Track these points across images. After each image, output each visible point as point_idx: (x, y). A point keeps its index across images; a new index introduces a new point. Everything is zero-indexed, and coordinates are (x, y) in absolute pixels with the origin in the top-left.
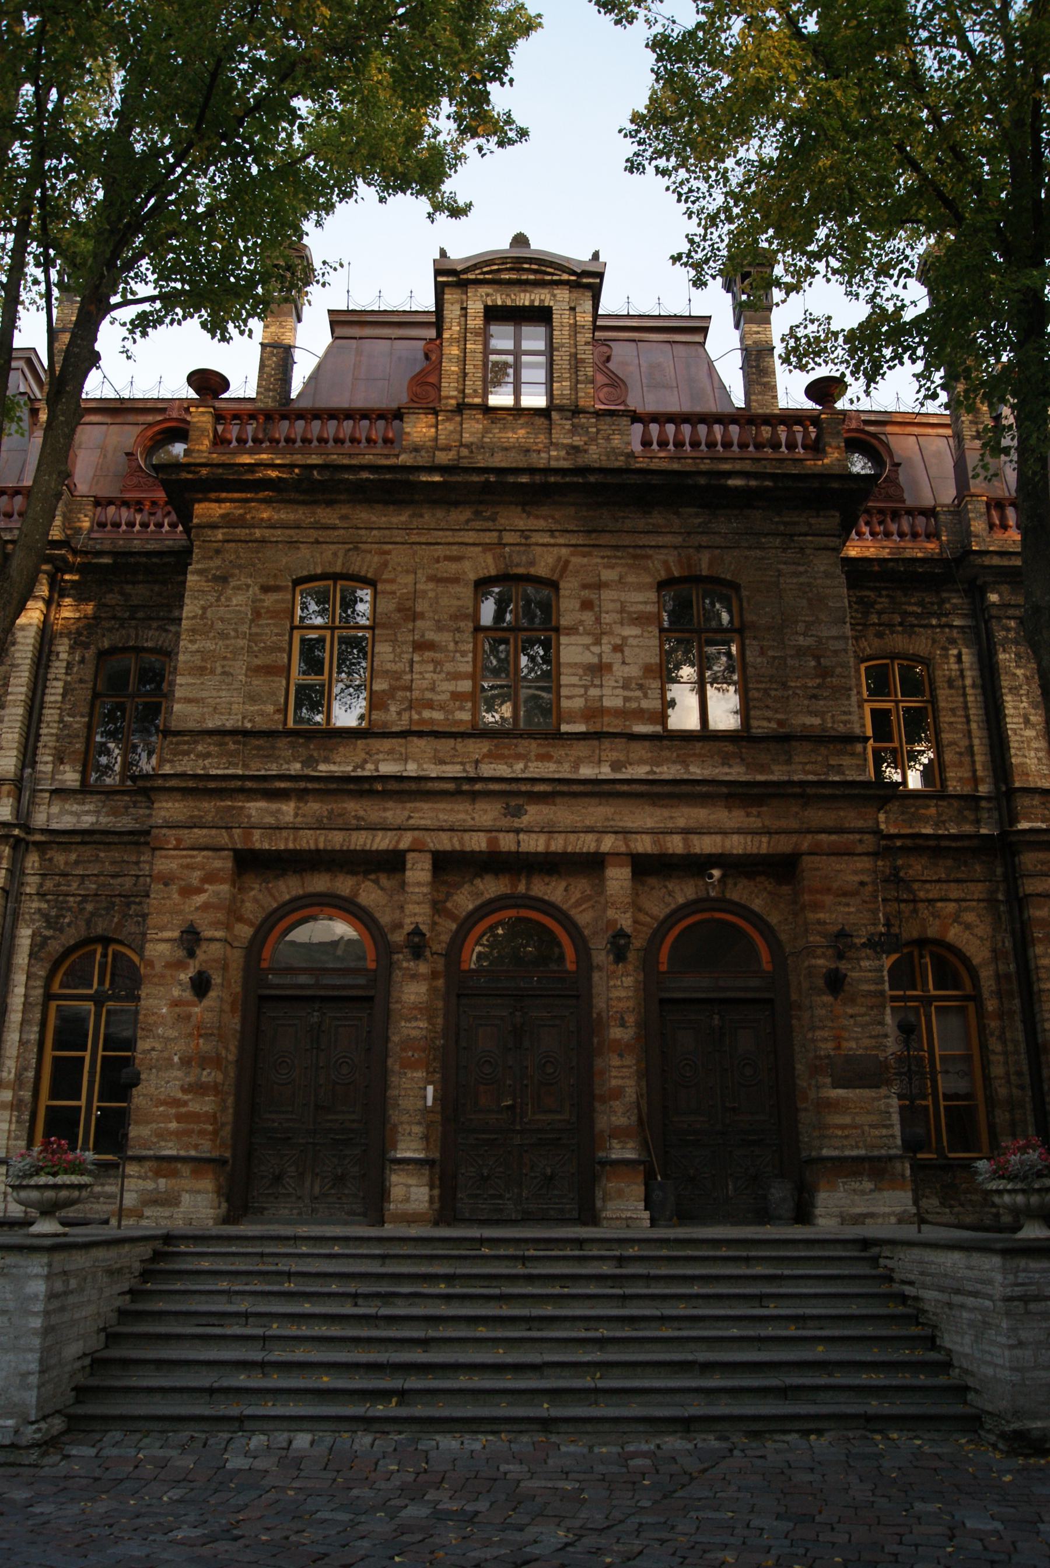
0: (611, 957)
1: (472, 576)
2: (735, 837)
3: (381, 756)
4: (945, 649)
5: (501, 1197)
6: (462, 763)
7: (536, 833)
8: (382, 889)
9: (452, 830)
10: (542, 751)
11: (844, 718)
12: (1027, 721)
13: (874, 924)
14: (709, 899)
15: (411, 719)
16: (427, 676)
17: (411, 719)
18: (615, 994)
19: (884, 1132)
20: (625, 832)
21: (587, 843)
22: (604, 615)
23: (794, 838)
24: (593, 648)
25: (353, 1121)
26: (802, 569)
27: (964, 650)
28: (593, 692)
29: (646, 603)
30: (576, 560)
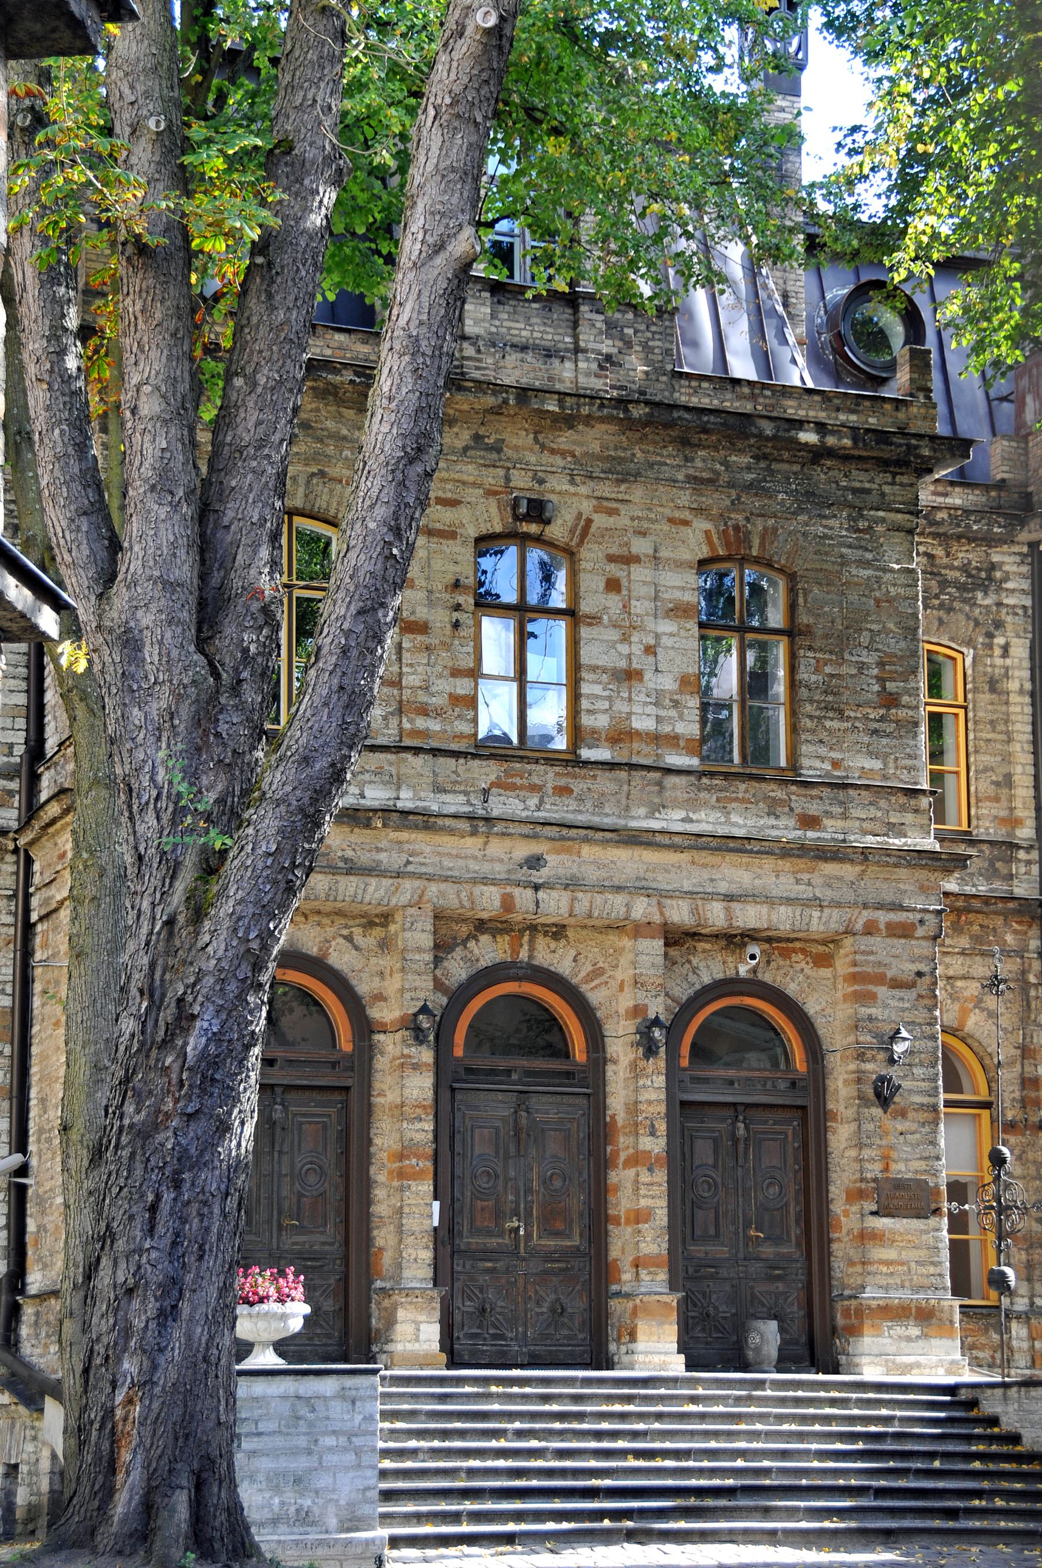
0: (641, 1050)
1: (472, 532)
2: (783, 909)
3: (367, 777)
4: (990, 636)
5: (502, 1337)
6: (466, 793)
8: (357, 948)
10: (562, 782)
11: (909, 762)
13: (930, 1024)
15: (401, 730)
16: (420, 669)
17: (401, 730)
18: (644, 1096)
19: (932, 1270)
22: (633, 602)
23: (847, 914)
24: (620, 647)
25: (324, 1243)
26: (869, 556)
27: (1014, 641)
28: (621, 707)
29: (683, 589)
30: (600, 521)
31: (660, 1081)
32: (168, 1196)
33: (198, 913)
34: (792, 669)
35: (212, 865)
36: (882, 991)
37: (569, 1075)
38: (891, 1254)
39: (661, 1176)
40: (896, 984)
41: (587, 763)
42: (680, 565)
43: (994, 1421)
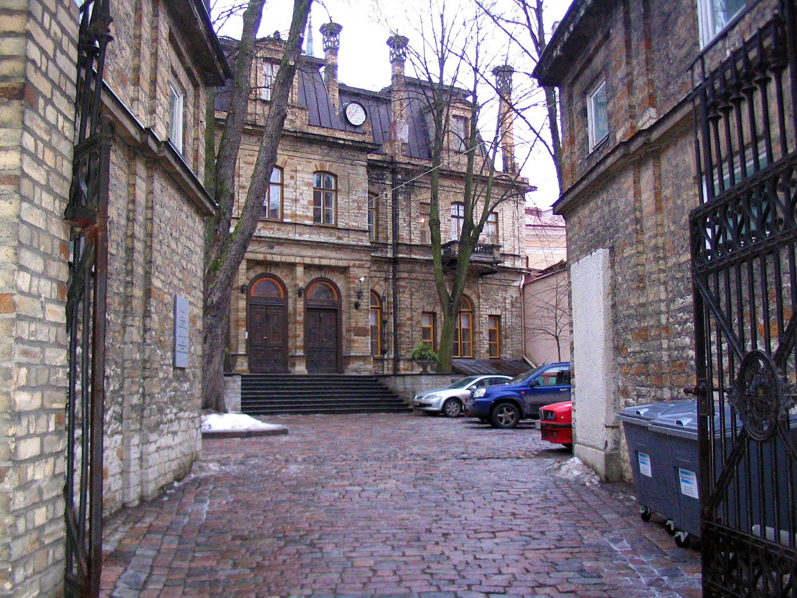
7: (278, 255)
20: (303, 257)
21: (292, 259)
28: (294, 208)
30: (289, 161)
31: (302, 303)
39: (302, 326)
41: (285, 223)
42: (308, 173)
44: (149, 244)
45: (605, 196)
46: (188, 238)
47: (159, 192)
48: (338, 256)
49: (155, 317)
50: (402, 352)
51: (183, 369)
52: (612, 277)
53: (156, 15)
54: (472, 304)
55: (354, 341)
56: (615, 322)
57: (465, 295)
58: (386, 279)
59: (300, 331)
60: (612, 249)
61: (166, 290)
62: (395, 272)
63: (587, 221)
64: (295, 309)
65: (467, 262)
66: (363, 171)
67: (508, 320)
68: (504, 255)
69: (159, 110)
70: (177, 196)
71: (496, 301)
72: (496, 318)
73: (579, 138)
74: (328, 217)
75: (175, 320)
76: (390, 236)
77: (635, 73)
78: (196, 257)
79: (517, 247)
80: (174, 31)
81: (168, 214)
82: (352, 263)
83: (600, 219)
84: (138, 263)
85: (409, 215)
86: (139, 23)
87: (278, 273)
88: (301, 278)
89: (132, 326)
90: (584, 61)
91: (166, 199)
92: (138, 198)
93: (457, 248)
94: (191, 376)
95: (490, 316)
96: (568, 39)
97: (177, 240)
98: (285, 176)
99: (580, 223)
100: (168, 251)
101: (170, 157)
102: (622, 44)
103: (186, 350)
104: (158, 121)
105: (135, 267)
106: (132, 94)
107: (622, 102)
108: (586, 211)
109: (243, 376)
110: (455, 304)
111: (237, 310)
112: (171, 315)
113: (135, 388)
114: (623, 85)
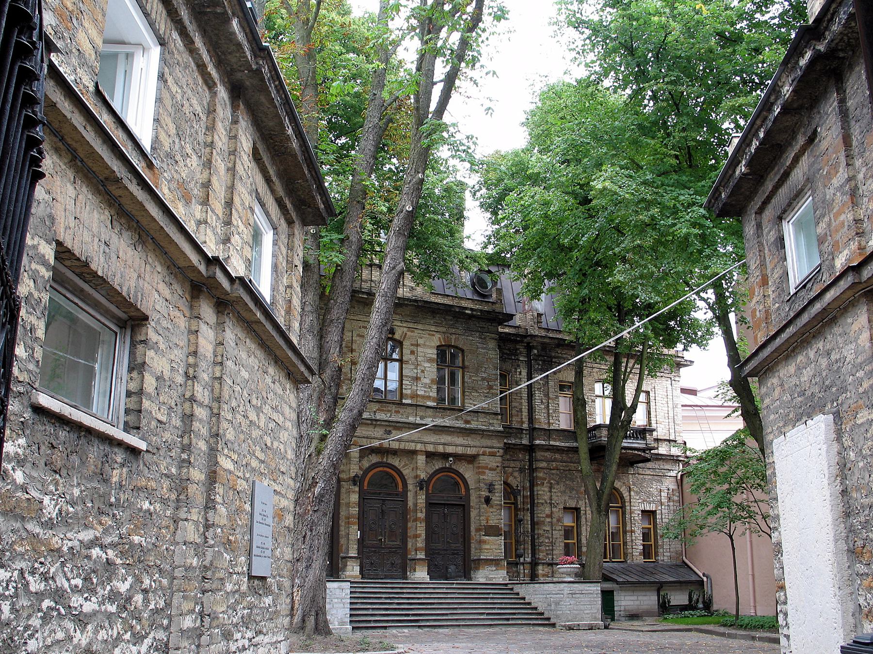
7: (394, 440)
9: (367, 438)
12: (542, 402)
14: (445, 468)
21: (412, 446)
23: (477, 449)
31: (424, 497)
32: (309, 533)
33: (319, 452)
34: (463, 378)
35: (323, 438)
36: (487, 471)
37: (397, 495)
38: (488, 547)
39: (424, 524)
40: (491, 469)
42: (431, 347)
43: (518, 594)
44: (215, 411)
45: (820, 345)
46: (274, 409)
47: (233, 344)
48: (465, 442)
49: (222, 509)
50: (541, 555)
51: (263, 579)
52: (839, 453)
53: (235, 122)
54: (622, 498)
55: (485, 542)
56: (847, 515)
57: (615, 489)
58: (521, 470)
59: (421, 530)
60: (838, 417)
61: (240, 474)
62: (531, 461)
63: (794, 380)
64: (416, 505)
65: (619, 449)
66: (492, 344)
67: (665, 516)
68: (657, 440)
69: (236, 239)
70: (259, 353)
71: (650, 494)
72: (649, 515)
73: (774, 277)
74: (453, 400)
75: (252, 515)
76: (525, 419)
77: (861, 176)
78: (286, 434)
79: (672, 431)
80: (261, 148)
81: (245, 374)
82: (481, 451)
83: (814, 376)
84: (198, 436)
85: (547, 395)
86: (211, 128)
87: (396, 462)
88: (422, 468)
89: (186, 520)
90: (778, 177)
91: (244, 355)
92: (201, 350)
93: (604, 432)
94: (275, 588)
95: (642, 511)
96: (757, 149)
97: (259, 410)
98: (404, 351)
99: (782, 385)
100: (245, 423)
101: (247, 299)
102: (839, 140)
103: (268, 553)
104: (232, 252)
105: (194, 441)
106: (198, 216)
107: (842, 217)
108: (792, 368)
109: (351, 582)
110: (605, 497)
111: (348, 505)
112: (247, 507)
113: (186, 606)
114: (843, 194)
